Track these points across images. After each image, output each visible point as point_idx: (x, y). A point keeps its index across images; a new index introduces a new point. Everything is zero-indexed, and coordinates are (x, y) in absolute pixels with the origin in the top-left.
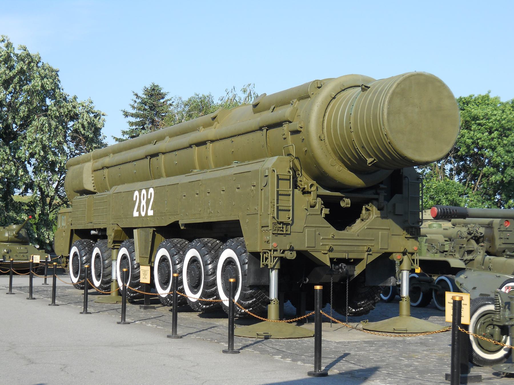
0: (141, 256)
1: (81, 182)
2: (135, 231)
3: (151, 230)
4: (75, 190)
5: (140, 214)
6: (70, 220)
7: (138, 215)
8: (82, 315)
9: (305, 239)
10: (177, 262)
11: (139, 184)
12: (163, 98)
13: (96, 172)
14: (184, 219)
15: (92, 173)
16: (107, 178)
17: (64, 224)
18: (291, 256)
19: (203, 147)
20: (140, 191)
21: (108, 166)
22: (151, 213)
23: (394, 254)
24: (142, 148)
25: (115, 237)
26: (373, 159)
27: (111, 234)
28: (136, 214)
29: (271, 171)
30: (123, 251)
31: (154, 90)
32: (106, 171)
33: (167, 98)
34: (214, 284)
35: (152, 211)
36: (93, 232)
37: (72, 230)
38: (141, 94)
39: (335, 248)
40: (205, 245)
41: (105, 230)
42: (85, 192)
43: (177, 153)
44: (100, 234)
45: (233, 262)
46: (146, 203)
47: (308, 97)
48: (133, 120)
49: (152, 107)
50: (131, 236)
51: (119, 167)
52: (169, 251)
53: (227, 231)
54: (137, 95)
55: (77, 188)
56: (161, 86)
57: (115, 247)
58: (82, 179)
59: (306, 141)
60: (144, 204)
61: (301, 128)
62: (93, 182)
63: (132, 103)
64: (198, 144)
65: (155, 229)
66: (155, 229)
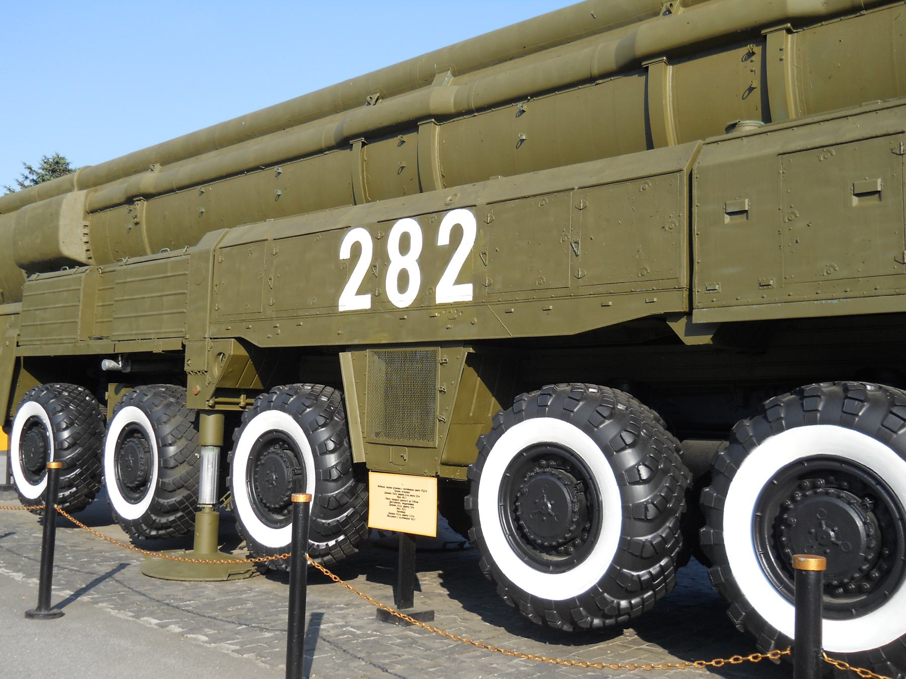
0: (374, 438)
1: (53, 237)
2: (346, 359)
5: (380, 298)
10: (64, 426)
13: (97, 215)
15: (85, 218)
16: (144, 226)
22: (452, 290)
25: (224, 378)
27: (206, 370)
28: (352, 300)
31: (57, 163)
32: (142, 206)
36: (107, 364)
37: (18, 359)
38: (36, 167)
40: (58, 395)
44: (128, 370)
46: (423, 261)
56: (69, 159)
57: (218, 407)
58: (56, 229)
60: (411, 266)
62: (86, 239)
66: (471, 350)
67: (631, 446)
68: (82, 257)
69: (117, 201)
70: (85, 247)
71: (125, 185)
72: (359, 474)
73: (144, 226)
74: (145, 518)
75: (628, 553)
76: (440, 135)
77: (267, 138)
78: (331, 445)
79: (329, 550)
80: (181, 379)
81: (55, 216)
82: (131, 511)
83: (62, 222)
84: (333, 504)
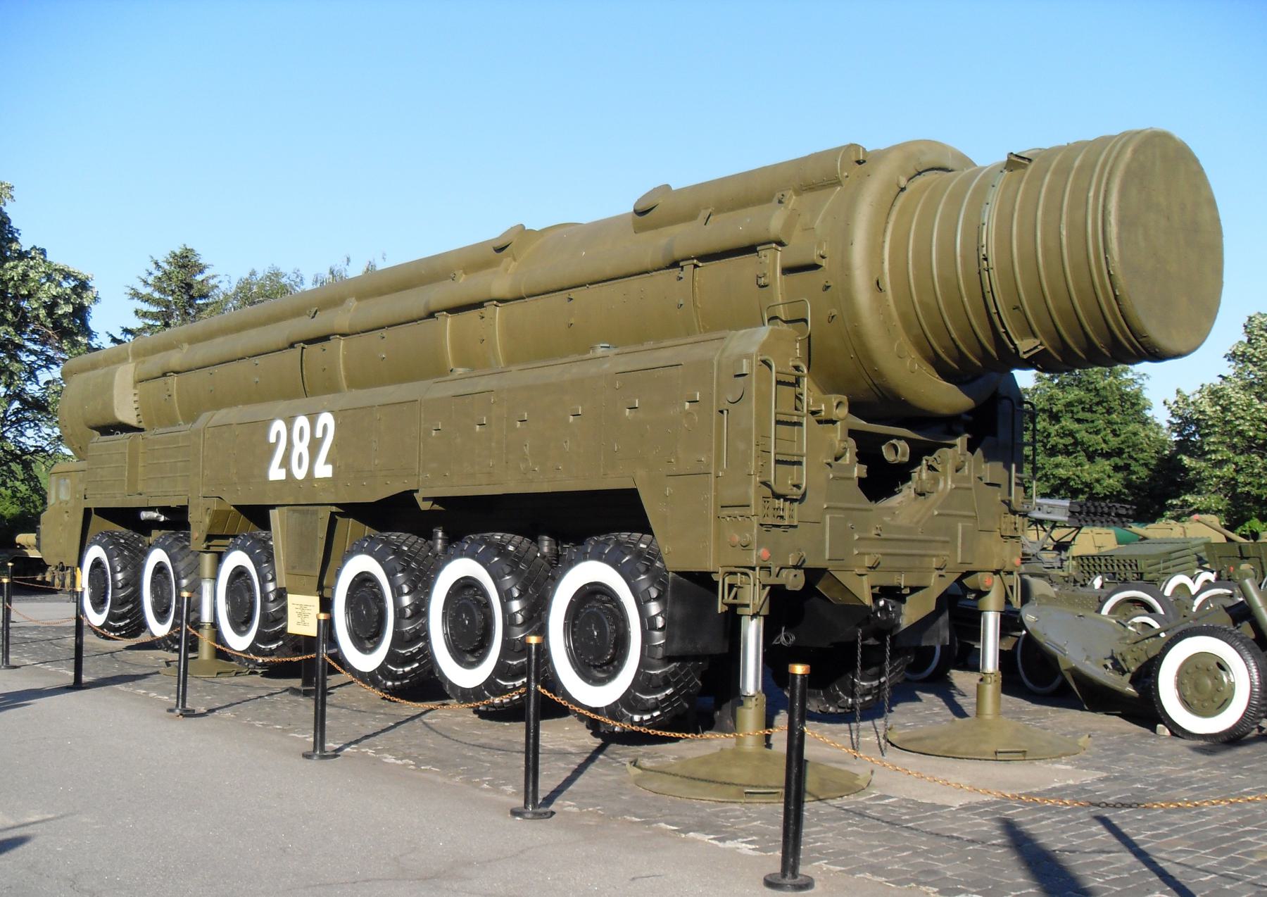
1: (108, 405)
2: (274, 515)
3: (325, 514)
4: (92, 424)
5: (289, 473)
6: (82, 487)
7: (329, 475)
8: (309, 762)
9: (823, 541)
11: (282, 405)
12: (201, 272)
14: (431, 487)
15: (135, 387)
16: (175, 397)
17: (64, 496)
18: (794, 581)
19: (473, 314)
20: (290, 423)
21: (178, 368)
22: (324, 470)
23: (979, 574)
24: (269, 328)
25: (211, 527)
26: (1038, 342)
27: (199, 522)
28: (276, 473)
29: (756, 360)
30: (237, 558)
32: (173, 381)
33: (208, 273)
34: (422, 635)
35: (330, 467)
36: (144, 515)
39: (885, 563)
40: (501, 549)
41: (183, 510)
42: (112, 428)
43: (384, 332)
45: (603, 593)
47: (835, 182)
48: (146, 307)
49: (181, 287)
50: (265, 524)
51: (211, 369)
52: (105, 549)
53: (603, 516)
54: (156, 263)
55: (99, 421)
56: (198, 250)
57: (212, 549)
59: (839, 291)
60: (302, 450)
61: (823, 257)
63: (144, 275)
64: (455, 310)
65: (334, 509)
67: (655, 599)
68: (133, 421)
69: (281, 346)
70: (136, 413)
71: (663, 242)
72: (281, 594)
73: (175, 397)
74: (382, 669)
75: (642, 682)
76: (452, 325)
77: (253, 333)
78: (406, 589)
79: (405, 675)
80: (186, 526)
81: (110, 386)
82: (367, 662)
83: (116, 392)
84: (271, 618)
